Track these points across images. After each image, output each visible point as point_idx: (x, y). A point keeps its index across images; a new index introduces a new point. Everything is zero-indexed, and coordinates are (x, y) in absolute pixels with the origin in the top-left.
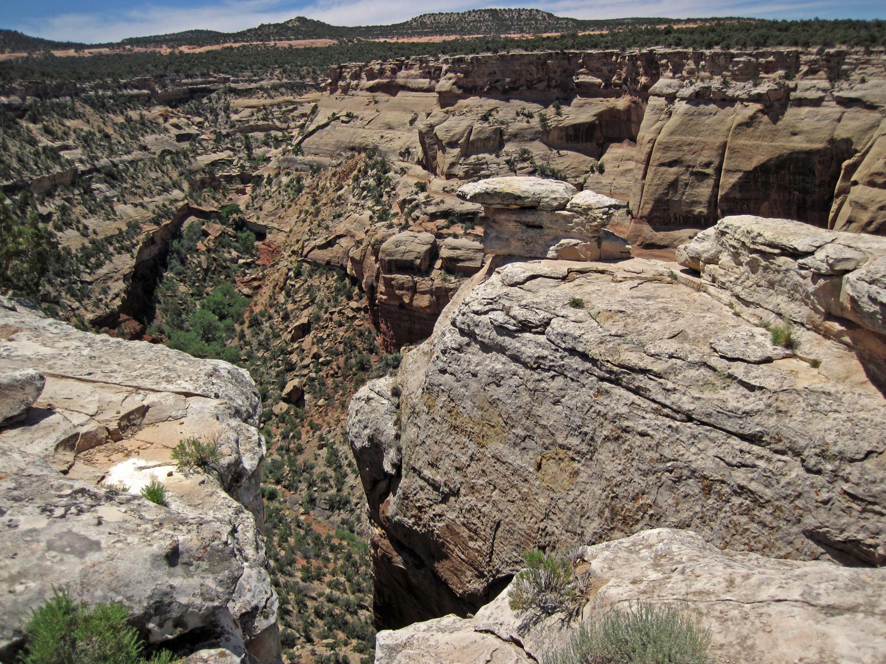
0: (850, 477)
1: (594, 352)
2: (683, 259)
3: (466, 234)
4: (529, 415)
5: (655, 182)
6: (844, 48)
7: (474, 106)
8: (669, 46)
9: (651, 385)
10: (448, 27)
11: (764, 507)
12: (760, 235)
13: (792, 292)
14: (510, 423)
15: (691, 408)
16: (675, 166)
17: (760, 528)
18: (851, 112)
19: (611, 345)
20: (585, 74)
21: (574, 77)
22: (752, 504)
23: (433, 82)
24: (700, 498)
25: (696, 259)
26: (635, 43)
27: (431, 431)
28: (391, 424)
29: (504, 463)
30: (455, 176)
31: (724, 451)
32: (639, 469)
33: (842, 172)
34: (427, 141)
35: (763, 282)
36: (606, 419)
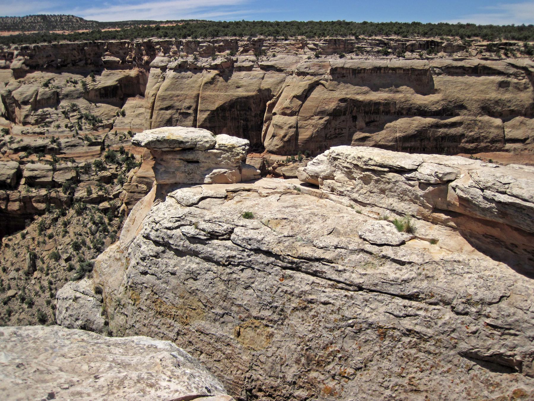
0: (491, 314)
1: (276, 249)
2: (303, 177)
3: (40, 161)
4: (225, 298)
5: (158, 120)
6: (262, 37)
7: (38, 78)
8: (160, 37)
9: (325, 268)
10: (13, 26)
11: (428, 341)
12: (370, 159)
13: (401, 195)
14: (208, 305)
15: (361, 282)
16: (170, 109)
17: (427, 355)
18: (269, 74)
19: (287, 244)
20: (109, 55)
21: (102, 58)
22: (418, 341)
23: (8, 62)
24: (378, 342)
25: (316, 176)
26: (139, 36)
27: (138, 317)
28: (99, 315)
29: (208, 335)
30: (29, 123)
31: (391, 307)
32: (326, 327)
33: (267, 108)
34: (8, 101)
35: (375, 190)
36: (293, 296)
